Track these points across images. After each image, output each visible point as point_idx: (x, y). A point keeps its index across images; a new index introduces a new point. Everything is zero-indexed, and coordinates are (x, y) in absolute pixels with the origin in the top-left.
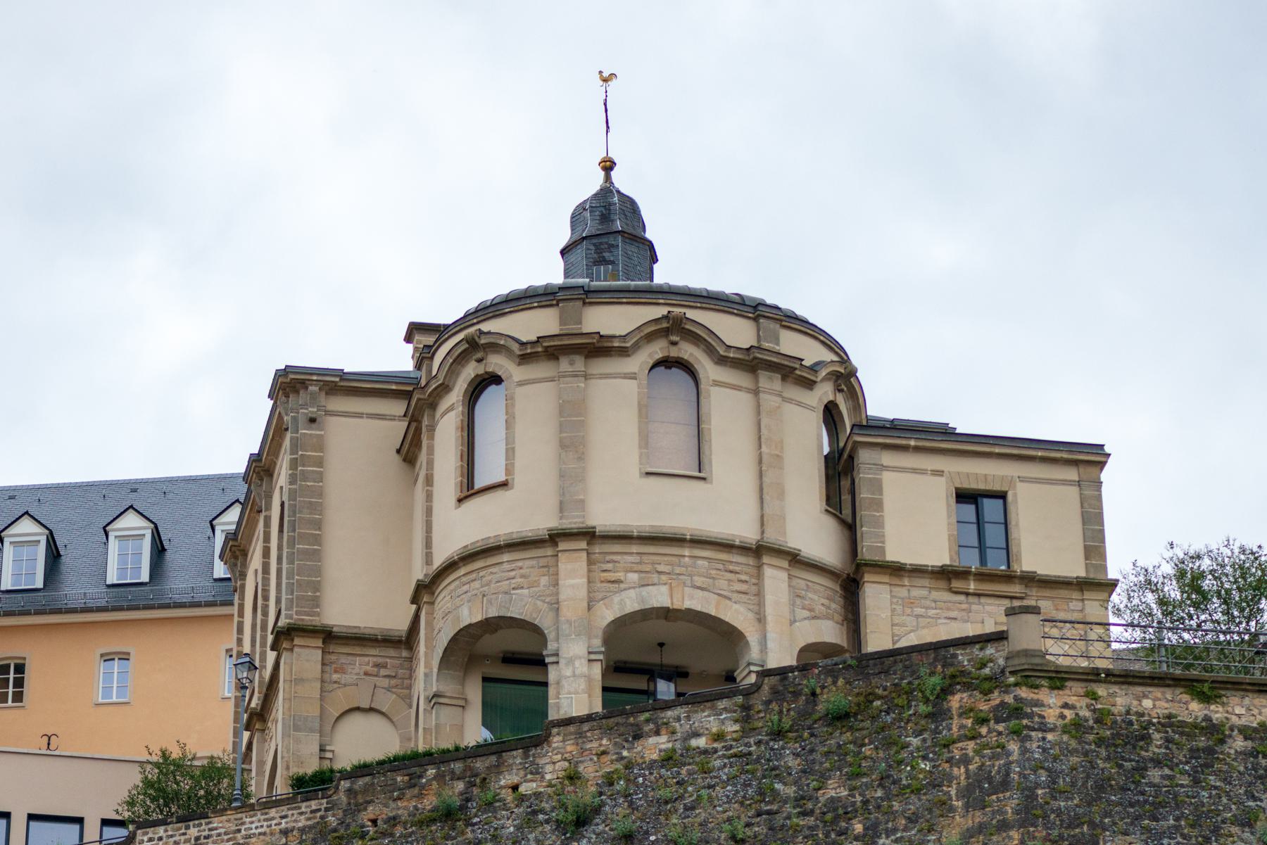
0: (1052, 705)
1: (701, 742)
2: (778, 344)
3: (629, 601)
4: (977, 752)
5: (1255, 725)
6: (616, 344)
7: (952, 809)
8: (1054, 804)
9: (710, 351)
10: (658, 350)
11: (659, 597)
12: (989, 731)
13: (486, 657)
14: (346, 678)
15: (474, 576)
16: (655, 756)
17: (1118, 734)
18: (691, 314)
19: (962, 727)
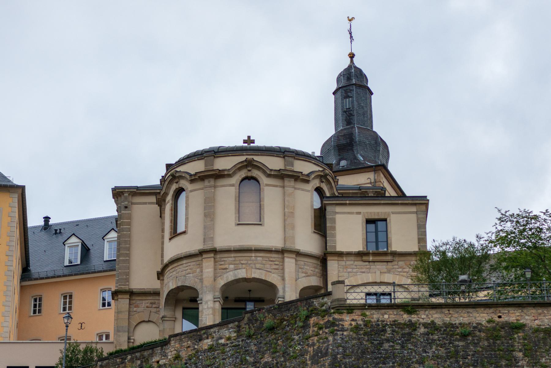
0: (347, 320)
1: (222, 341)
2: (293, 167)
3: (230, 276)
4: (318, 341)
5: (429, 322)
6: (226, 173)
7: (307, 365)
8: (344, 361)
9: (264, 172)
10: (243, 174)
11: (242, 274)
12: (323, 332)
13: (184, 300)
14: (139, 310)
15: (173, 270)
16: (206, 348)
17: (373, 330)
18: (256, 158)
19: (313, 331)
